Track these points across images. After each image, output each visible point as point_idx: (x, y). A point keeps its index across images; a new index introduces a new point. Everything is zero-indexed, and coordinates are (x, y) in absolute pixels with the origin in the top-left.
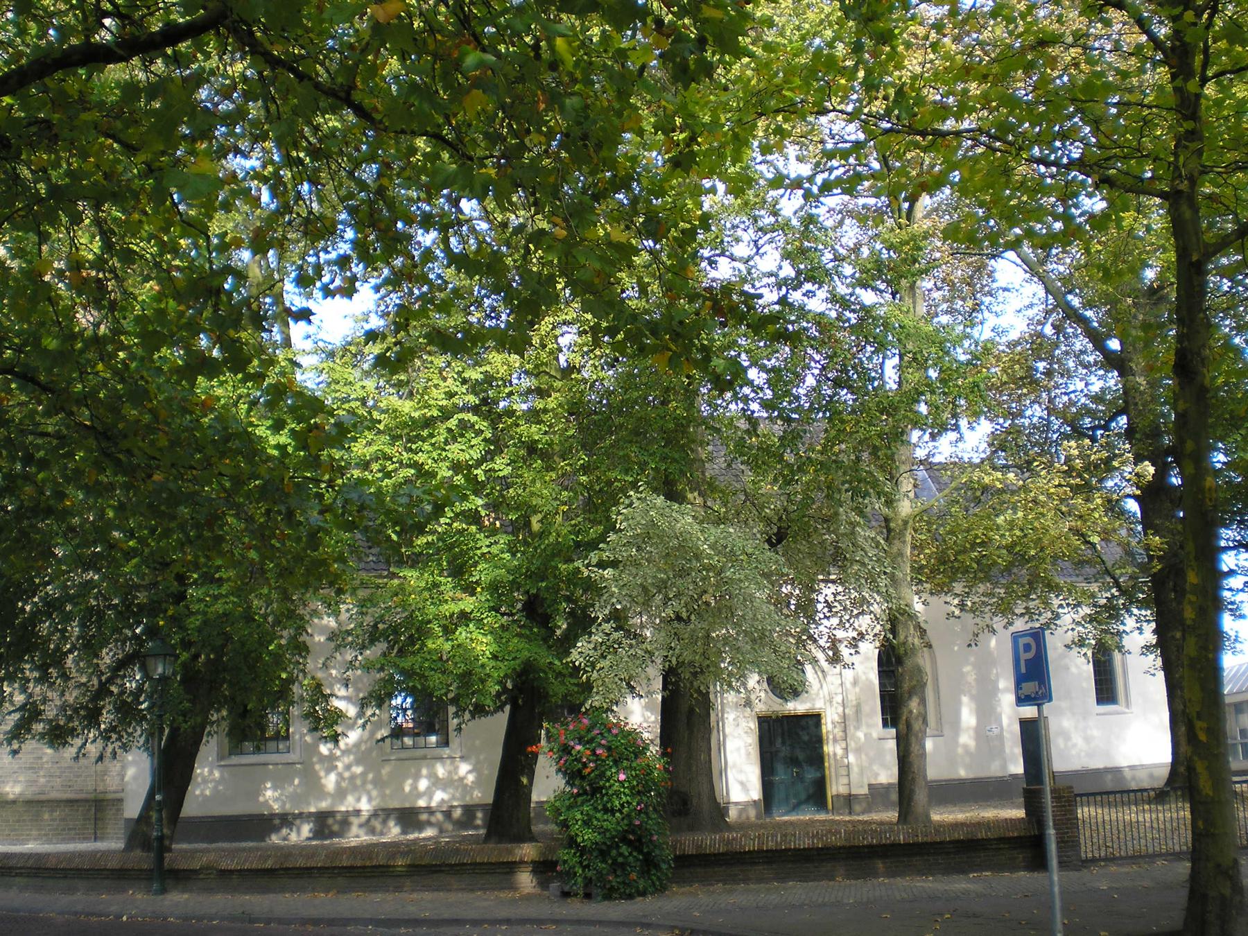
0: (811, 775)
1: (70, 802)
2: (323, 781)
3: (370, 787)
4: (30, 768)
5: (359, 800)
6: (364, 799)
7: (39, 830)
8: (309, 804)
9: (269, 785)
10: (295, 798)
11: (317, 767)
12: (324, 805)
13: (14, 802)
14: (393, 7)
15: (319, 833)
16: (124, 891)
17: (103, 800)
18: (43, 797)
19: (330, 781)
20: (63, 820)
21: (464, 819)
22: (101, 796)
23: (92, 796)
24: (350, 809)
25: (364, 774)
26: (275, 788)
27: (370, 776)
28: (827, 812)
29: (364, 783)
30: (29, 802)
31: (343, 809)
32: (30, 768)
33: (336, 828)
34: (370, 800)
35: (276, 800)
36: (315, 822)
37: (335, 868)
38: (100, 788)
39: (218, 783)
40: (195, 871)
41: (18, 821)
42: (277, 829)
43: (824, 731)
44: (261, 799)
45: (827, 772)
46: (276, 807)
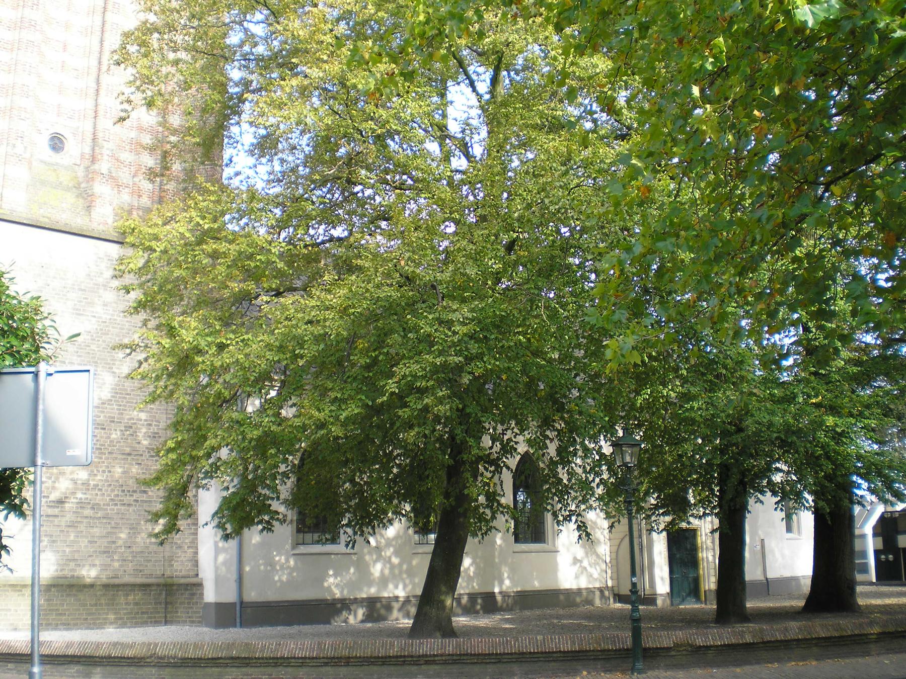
0: (692, 575)
1: (145, 587)
2: (372, 570)
3: (405, 576)
4: (105, 552)
5: (396, 587)
6: (401, 586)
7: (115, 613)
8: (361, 590)
9: (331, 572)
10: (351, 585)
11: (367, 558)
12: (373, 591)
13: (92, 586)
14: (81, 297)
15: (368, 618)
16: (576, 672)
17: (173, 585)
18: (117, 581)
19: (377, 569)
20: (136, 604)
21: (469, 605)
22: (169, 581)
23: (162, 581)
24: (391, 595)
25: (400, 564)
26: (335, 575)
27: (405, 567)
28: (701, 603)
29: (401, 572)
30: (106, 586)
31: (386, 595)
32: (105, 552)
33: (383, 612)
34: (405, 586)
35: (337, 586)
36: (367, 607)
37: (813, 639)
38: (168, 573)
39: (293, 570)
40: (668, 649)
41: (96, 605)
42: (338, 612)
43: (699, 541)
44: (326, 584)
45: (701, 572)
46: (338, 594)
